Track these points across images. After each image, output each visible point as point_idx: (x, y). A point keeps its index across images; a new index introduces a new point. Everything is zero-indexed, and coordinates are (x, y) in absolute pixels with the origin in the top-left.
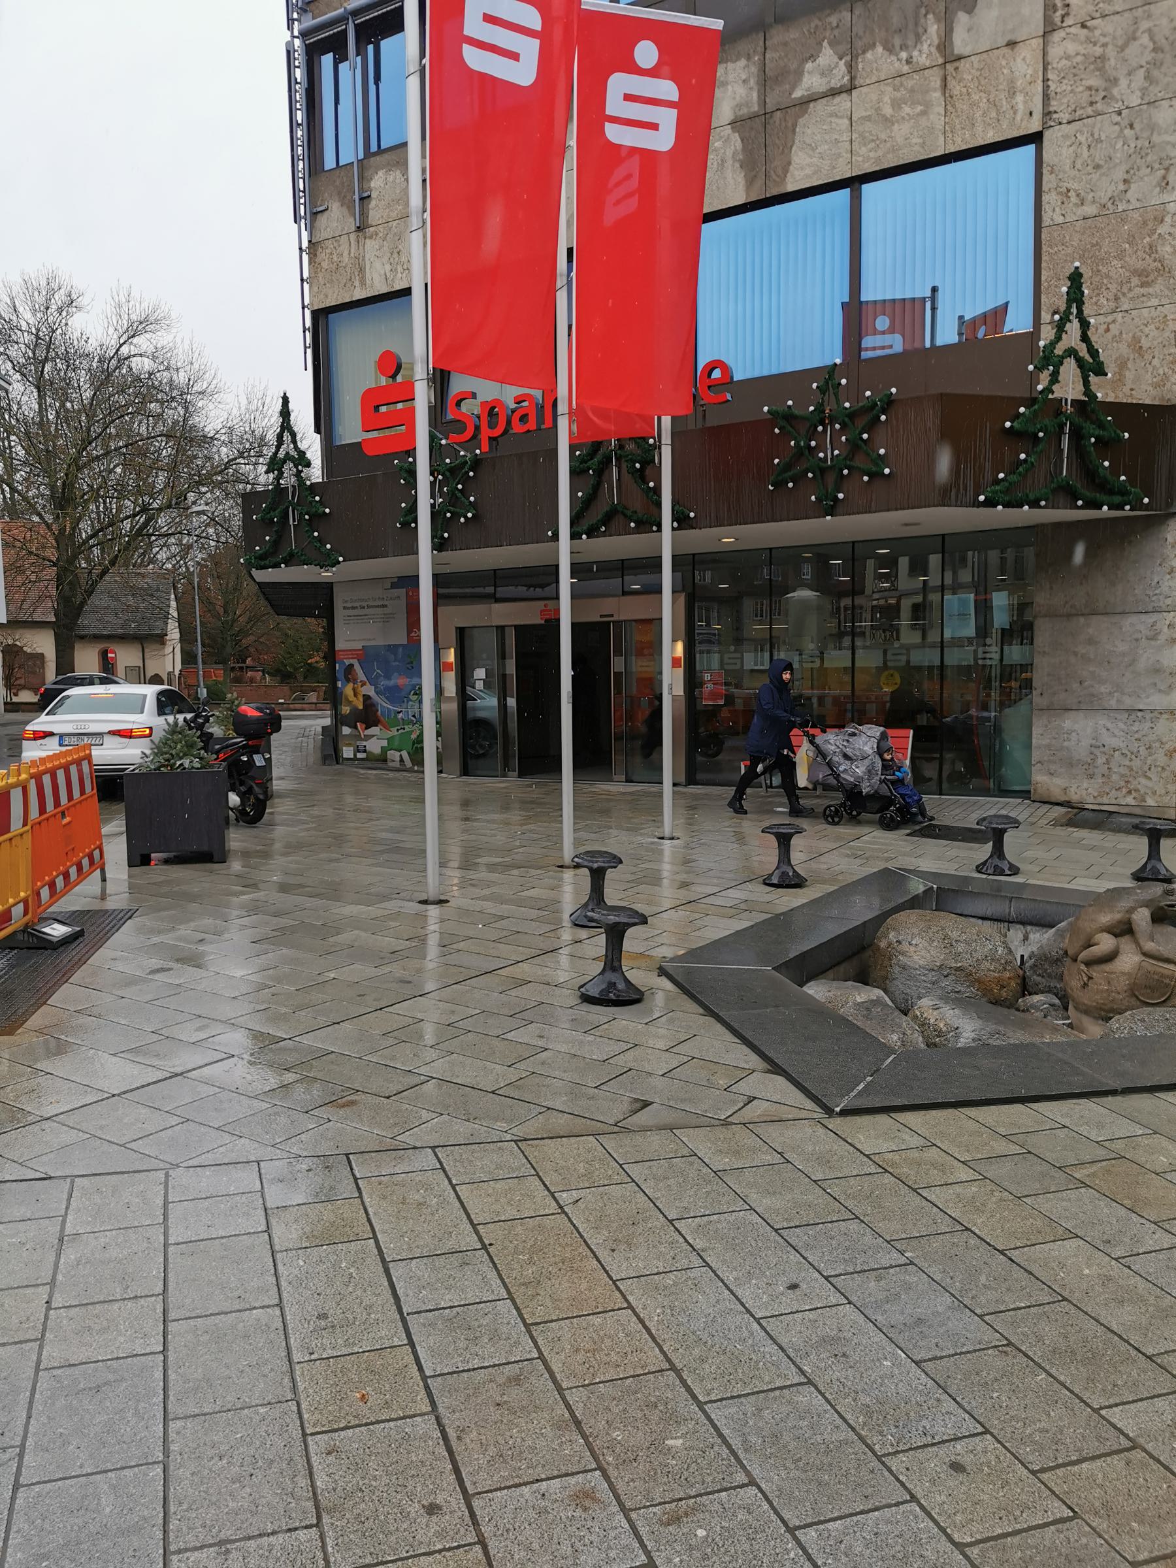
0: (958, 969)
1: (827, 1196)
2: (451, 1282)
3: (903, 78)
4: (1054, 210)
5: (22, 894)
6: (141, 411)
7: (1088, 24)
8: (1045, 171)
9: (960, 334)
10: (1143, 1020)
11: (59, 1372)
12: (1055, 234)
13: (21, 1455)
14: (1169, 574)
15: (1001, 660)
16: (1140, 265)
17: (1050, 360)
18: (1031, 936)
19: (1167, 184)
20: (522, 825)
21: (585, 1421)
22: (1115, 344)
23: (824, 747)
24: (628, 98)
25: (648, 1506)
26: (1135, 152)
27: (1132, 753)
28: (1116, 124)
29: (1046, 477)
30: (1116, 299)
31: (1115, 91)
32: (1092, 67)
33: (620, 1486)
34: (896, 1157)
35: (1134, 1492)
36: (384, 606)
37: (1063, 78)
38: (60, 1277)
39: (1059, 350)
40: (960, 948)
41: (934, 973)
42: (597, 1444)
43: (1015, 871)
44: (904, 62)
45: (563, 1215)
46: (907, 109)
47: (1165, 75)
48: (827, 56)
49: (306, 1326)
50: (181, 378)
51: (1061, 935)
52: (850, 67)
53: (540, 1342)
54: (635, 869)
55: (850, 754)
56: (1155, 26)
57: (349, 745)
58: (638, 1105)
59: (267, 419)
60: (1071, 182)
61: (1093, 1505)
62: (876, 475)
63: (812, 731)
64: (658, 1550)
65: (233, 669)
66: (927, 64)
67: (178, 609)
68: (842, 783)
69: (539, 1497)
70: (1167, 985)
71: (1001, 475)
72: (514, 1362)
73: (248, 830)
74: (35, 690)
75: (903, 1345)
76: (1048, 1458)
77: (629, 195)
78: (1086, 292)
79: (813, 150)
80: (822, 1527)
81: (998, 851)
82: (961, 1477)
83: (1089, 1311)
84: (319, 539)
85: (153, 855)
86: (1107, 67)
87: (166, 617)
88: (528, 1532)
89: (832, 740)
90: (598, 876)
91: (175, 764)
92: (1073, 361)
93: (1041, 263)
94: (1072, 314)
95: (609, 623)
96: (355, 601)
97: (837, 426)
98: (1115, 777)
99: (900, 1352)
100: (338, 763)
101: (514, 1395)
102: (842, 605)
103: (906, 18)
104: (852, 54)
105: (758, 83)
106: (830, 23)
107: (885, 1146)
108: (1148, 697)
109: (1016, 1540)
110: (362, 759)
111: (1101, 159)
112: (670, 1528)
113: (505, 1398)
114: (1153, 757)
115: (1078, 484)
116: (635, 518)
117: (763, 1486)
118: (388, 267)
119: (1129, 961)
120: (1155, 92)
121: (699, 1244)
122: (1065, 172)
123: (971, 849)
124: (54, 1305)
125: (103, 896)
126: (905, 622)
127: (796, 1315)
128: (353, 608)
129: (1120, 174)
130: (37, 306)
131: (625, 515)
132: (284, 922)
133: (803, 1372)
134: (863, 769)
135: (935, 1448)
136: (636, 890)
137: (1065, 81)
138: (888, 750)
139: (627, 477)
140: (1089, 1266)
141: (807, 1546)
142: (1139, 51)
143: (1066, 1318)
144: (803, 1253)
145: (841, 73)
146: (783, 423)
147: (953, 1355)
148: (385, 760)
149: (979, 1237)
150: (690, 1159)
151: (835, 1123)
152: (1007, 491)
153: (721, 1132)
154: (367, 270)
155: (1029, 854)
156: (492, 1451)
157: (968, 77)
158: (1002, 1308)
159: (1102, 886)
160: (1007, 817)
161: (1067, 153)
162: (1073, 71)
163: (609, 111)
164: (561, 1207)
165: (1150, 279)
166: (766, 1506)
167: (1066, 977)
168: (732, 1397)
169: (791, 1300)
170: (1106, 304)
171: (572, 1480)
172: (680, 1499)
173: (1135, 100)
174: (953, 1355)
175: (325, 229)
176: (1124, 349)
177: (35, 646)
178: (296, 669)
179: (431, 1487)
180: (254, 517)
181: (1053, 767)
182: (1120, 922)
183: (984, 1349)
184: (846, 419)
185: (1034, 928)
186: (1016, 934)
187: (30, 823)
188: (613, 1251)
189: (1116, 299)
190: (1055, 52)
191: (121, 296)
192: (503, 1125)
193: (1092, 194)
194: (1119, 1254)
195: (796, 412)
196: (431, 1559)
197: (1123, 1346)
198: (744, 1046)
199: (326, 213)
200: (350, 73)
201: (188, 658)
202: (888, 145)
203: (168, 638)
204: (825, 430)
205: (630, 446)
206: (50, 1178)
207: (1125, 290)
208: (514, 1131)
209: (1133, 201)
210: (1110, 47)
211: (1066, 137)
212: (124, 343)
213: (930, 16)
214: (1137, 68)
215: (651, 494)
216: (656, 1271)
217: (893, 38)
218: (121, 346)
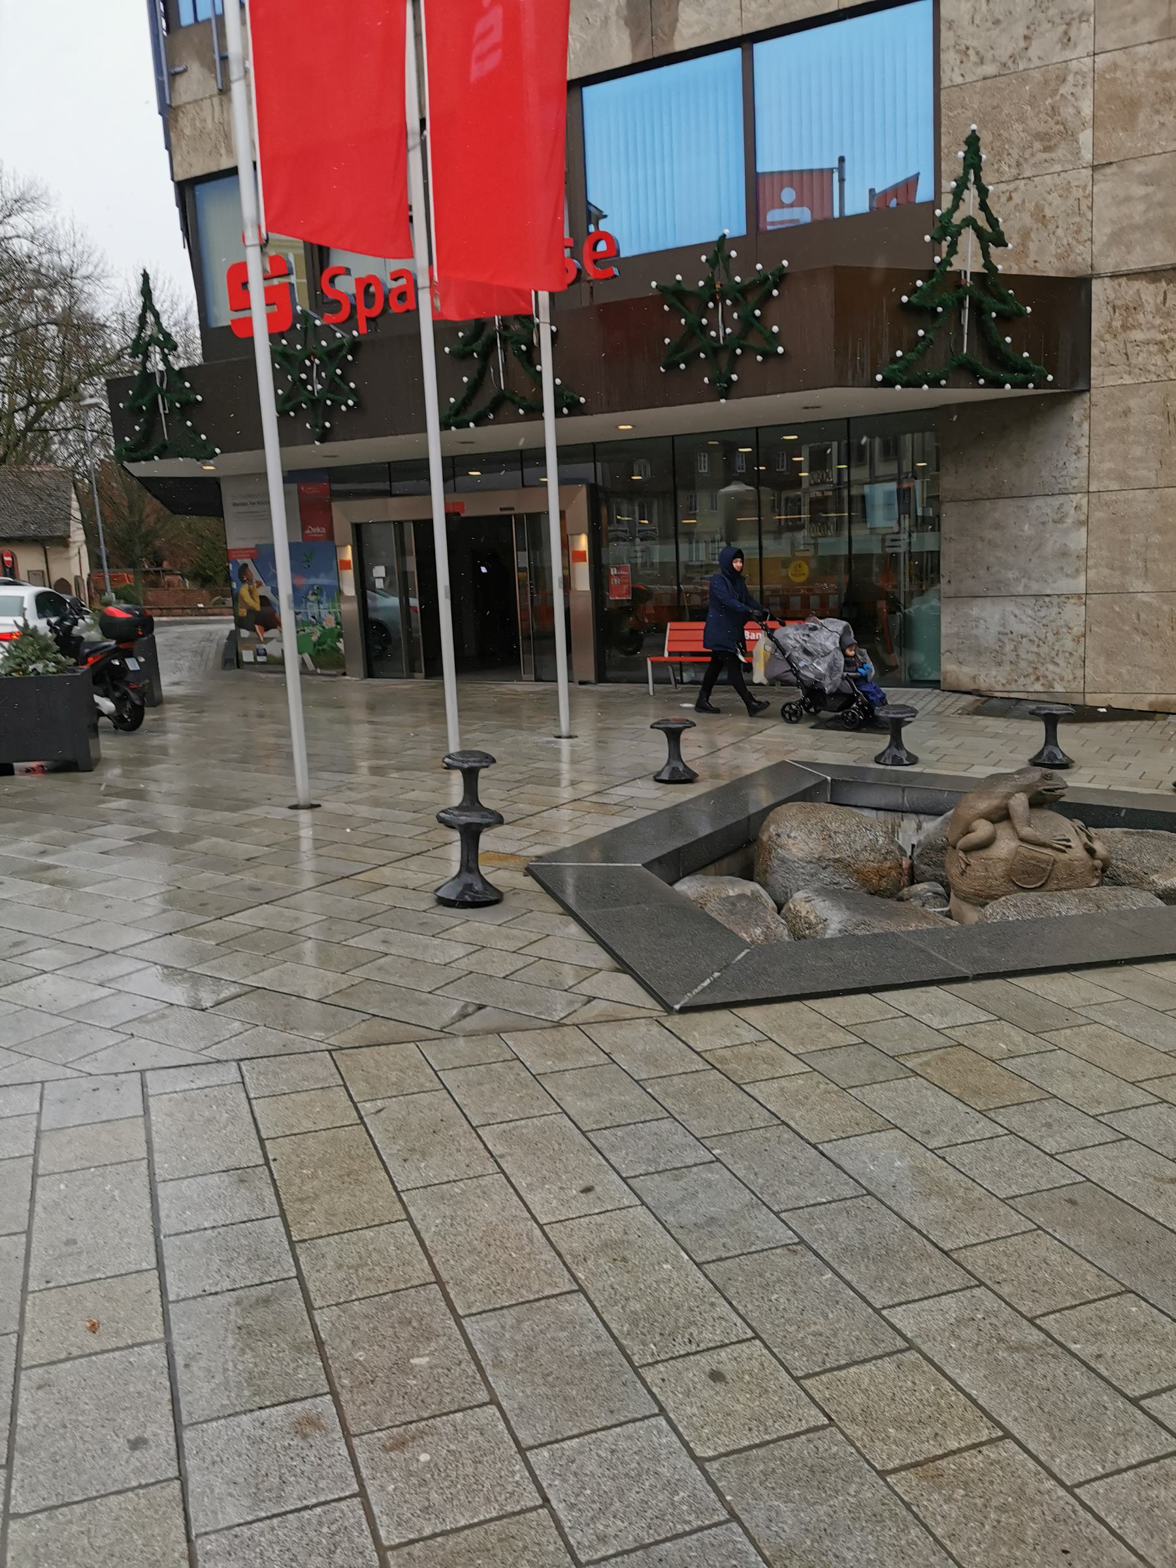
0: (837, 861)
1: (645, 1096)
6: (27, 301)
8: (943, 27)
10: (1015, 906)
16: (1042, 128)
17: (947, 230)
19: (1069, 40)
30: (1018, 165)
33: (349, 1411)
34: (727, 1053)
35: (899, 1395)
39: (957, 218)
40: (839, 839)
43: (913, 760)
45: (362, 1126)
50: (65, 261)
53: (302, 1259)
54: (524, 769)
55: (811, 650)
57: (247, 648)
61: (852, 1411)
62: (769, 355)
65: (147, 572)
67: (81, 510)
70: (1044, 870)
75: (688, 1247)
76: (815, 1363)
78: (984, 157)
80: (557, 1446)
81: (897, 742)
85: (16, 765)
87: (68, 517)
89: (791, 634)
90: (470, 777)
93: (940, 127)
94: (969, 180)
95: (510, 516)
97: (728, 302)
98: (1023, 664)
99: (683, 1254)
102: (783, 497)
108: (1054, 582)
109: (761, 1452)
112: (392, 1454)
115: (979, 361)
119: (1005, 846)
121: (497, 1150)
123: (874, 740)
129: (1020, 30)
131: (513, 402)
133: (575, 1279)
134: (826, 665)
135: (698, 1357)
136: (521, 790)
139: (515, 363)
140: (901, 1158)
146: (674, 300)
151: (675, 1022)
152: (906, 370)
158: (802, 1204)
160: (904, 706)
164: (361, 1118)
165: (1052, 143)
166: (501, 1426)
167: (948, 866)
168: (494, 1310)
169: (584, 1204)
170: (1008, 171)
171: (298, 1406)
172: (411, 1422)
181: (961, 656)
182: (997, 808)
184: (738, 295)
185: (927, 817)
186: (909, 824)
188: (405, 1160)
189: (1018, 165)
192: (320, 1035)
193: (991, 52)
195: (687, 287)
197: (920, 1241)
199: (185, 76)
204: (716, 306)
205: (515, 327)
207: (1027, 155)
208: (331, 1041)
216: (446, 1179)
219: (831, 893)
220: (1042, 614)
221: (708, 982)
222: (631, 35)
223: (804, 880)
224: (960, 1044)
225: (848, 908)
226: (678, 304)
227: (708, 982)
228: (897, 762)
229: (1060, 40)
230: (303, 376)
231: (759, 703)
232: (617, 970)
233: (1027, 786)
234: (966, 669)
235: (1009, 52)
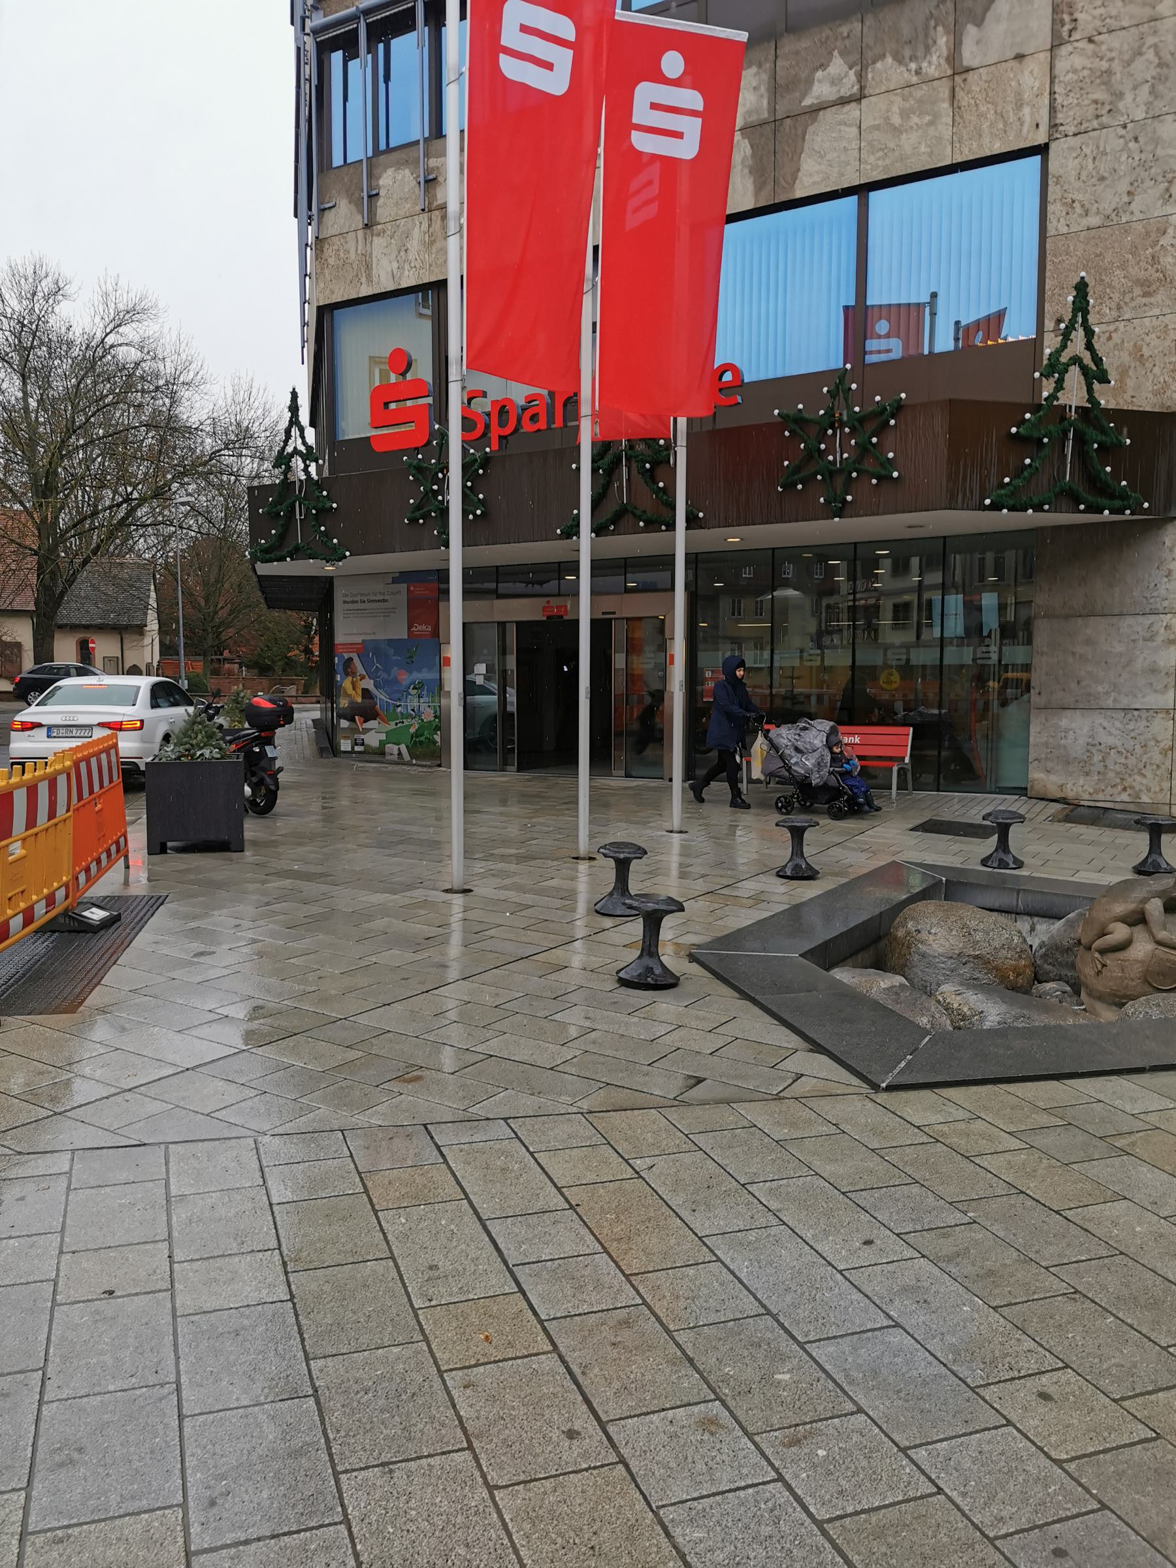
0: (976, 957)
1: (885, 1163)
2: (547, 1237)
3: (912, 89)
4: (1059, 221)
5: (64, 878)
7: (1096, 39)
9: (956, 339)
10: (1158, 1005)
11: (196, 1318)
12: (1060, 244)
13: (178, 1390)
14: (1167, 576)
15: (1000, 661)
16: (1142, 275)
17: (1056, 368)
18: (1038, 927)
19: (1170, 196)
20: (530, 818)
21: (696, 1359)
22: (1116, 352)
23: (777, 741)
24: (654, 106)
25: (769, 1431)
26: (1139, 165)
27: (1128, 751)
28: (1121, 137)
29: (1049, 483)
30: (1119, 308)
31: (1121, 105)
32: (1098, 81)
33: (740, 1414)
36: (384, 601)
37: (1070, 91)
38: (175, 1234)
39: (1064, 358)
40: (979, 936)
41: (953, 961)
42: (712, 1378)
43: (1019, 864)
44: (913, 73)
46: (915, 119)
47: (1170, 89)
48: (837, 65)
49: (420, 1275)
50: (167, 369)
51: (1071, 925)
52: (860, 77)
56: (1161, 41)
57: (346, 738)
58: (693, 1081)
59: (253, 411)
60: (1076, 193)
62: (884, 478)
63: (766, 727)
64: (785, 1467)
66: (937, 76)
68: (793, 776)
69: (668, 1423)
71: (1007, 480)
72: (621, 1308)
73: (261, 821)
74: (11, 678)
75: (979, 1294)
77: (647, 203)
78: (1091, 301)
79: (822, 157)
82: (1050, 1405)
83: (1146, 1263)
84: (325, 533)
86: (1113, 81)
88: (663, 1453)
89: (784, 735)
90: (623, 867)
91: (195, 754)
92: (1078, 369)
94: (1076, 322)
95: (611, 619)
96: (356, 595)
97: (847, 430)
98: (1111, 775)
99: (976, 1299)
100: (335, 756)
101: (625, 1335)
103: (916, 30)
104: (862, 64)
105: (768, 90)
106: (841, 34)
107: (933, 1119)
108: (1144, 697)
109: (1108, 1456)
110: (360, 752)
111: (1105, 171)
113: (619, 1339)
114: (1149, 755)
116: (644, 518)
117: (871, 1413)
118: (395, 265)
119: (1142, 948)
120: (1160, 106)
121: (773, 1205)
122: (1070, 183)
123: (961, 842)
124: (176, 1259)
125: (126, 883)
126: (886, 621)
127: (875, 1267)
128: (353, 602)
129: (1124, 186)
130: (23, 293)
132: (315, 909)
133: (890, 1317)
135: (1022, 1381)
137: (1071, 95)
138: (836, 744)
139: (637, 478)
140: (1140, 1224)
141: (920, 1463)
142: (1144, 67)
143: (1125, 1269)
144: (872, 1213)
145: (851, 83)
146: (793, 426)
147: (1026, 1302)
148: (383, 754)
149: (1034, 1199)
150: (751, 1130)
151: (882, 1097)
152: (1012, 494)
153: (774, 1106)
154: (374, 266)
155: (1030, 848)
156: (616, 1385)
157: (976, 88)
159: (1114, 879)
161: (1072, 164)
162: (1080, 84)
163: (635, 120)
164: (637, 1173)
165: (1151, 289)
168: (828, 1338)
169: (867, 1255)
170: (1108, 313)
171: (696, 1409)
172: (797, 1425)
173: (1139, 114)
174: (1026, 1302)
175: (332, 226)
176: (1125, 357)
177: (15, 634)
178: (274, 662)
179: (567, 1415)
180: (260, 511)
181: (1049, 765)
182: (1134, 912)
183: (1054, 1296)
184: (856, 424)
185: (1041, 920)
186: (1024, 924)
187: (72, 809)
188: (694, 1211)
189: (1119, 308)
190: (1061, 66)
191: (109, 284)
193: (1096, 205)
194: (1166, 1214)
195: (806, 415)
196: (579, 1476)
198: (783, 1028)
199: (333, 210)
200: (361, 72)
201: (167, 649)
202: (897, 153)
203: (147, 629)
204: (834, 434)
205: (640, 447)
206: (145, 1145)
209: (1137, 213)
210: (1116, 61)
211: (1071, 149)
212: (111, 332)
213: (940, 29)
214: (1143, 83)
215: (661, 494)
216: (737, 1229)
217: (903, 48)
218: (107, 335)
219: (972, 984)
220: (1131, 727)
221: (903, 1064)
222: (754, 182)
223: (944, 974)
224: (1157, 1128)
225: (1005, 1002)
226: (799, 431)
227: (903, 1064)
228: (1003, 865)
229: (1162, 196)
230: (435, 487)
231: (743, 801)
232: (811, 1051)
233: (1163, 891)
234: (1053, 778)
235: (1113, 206)
